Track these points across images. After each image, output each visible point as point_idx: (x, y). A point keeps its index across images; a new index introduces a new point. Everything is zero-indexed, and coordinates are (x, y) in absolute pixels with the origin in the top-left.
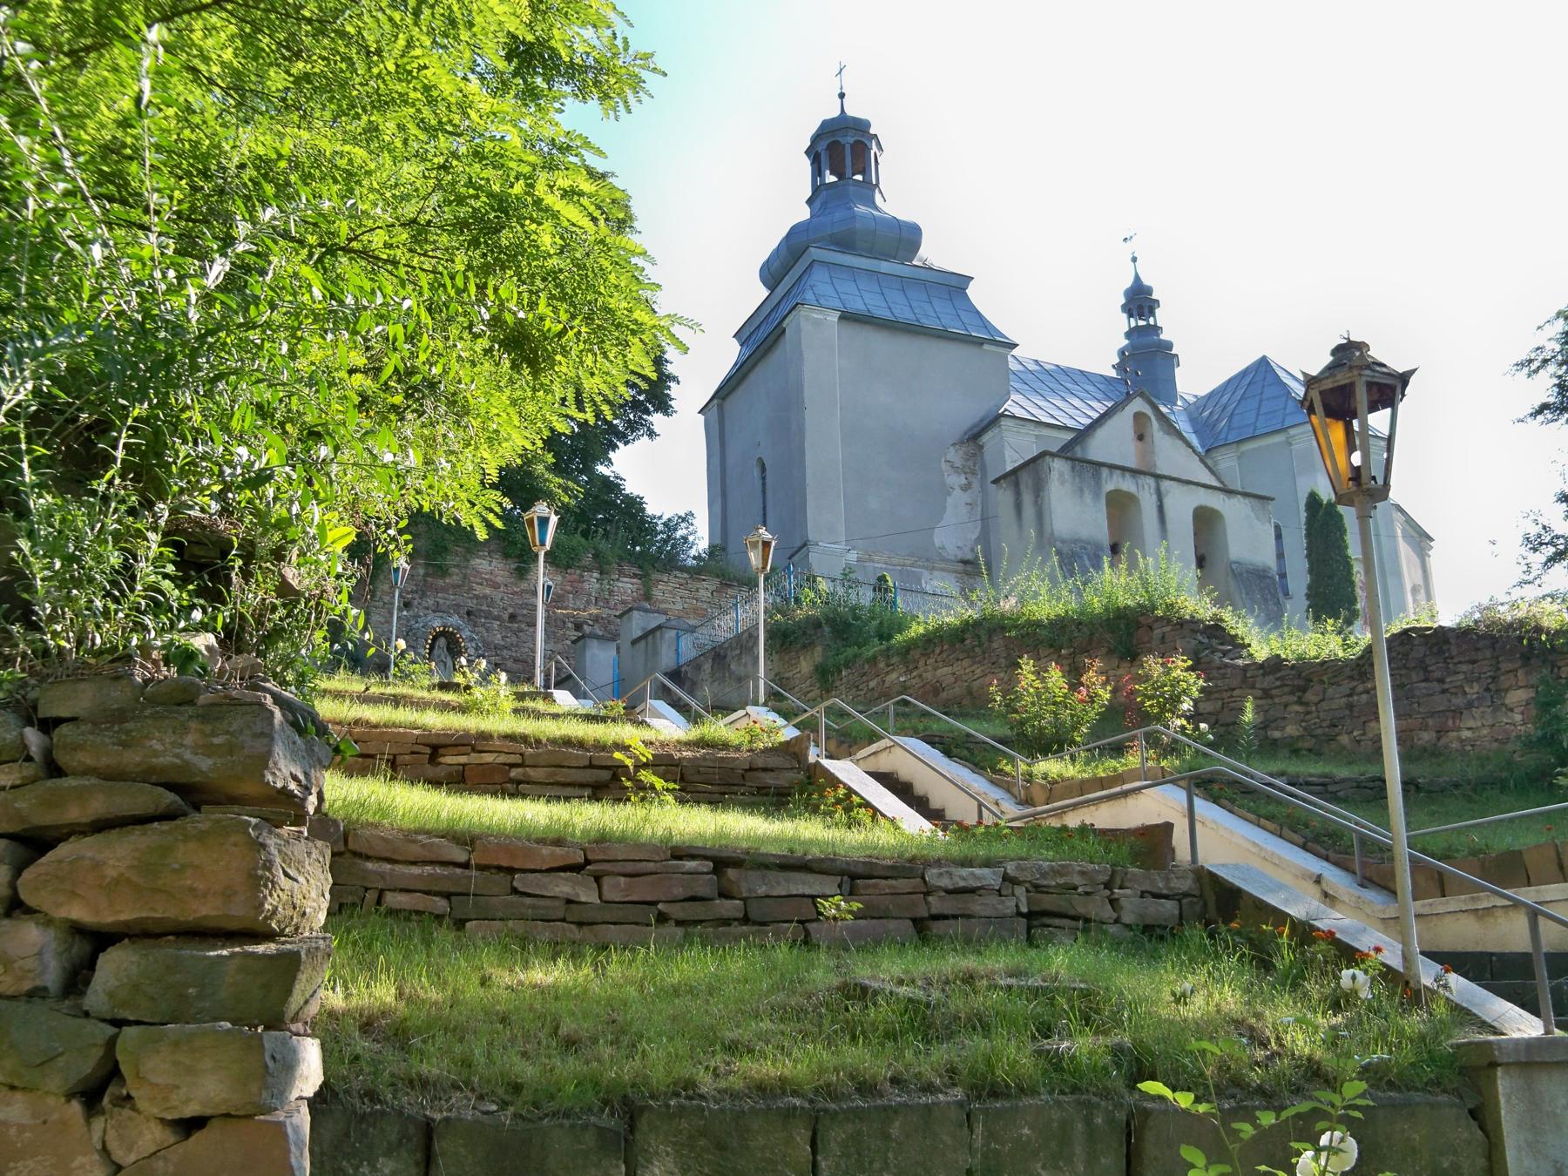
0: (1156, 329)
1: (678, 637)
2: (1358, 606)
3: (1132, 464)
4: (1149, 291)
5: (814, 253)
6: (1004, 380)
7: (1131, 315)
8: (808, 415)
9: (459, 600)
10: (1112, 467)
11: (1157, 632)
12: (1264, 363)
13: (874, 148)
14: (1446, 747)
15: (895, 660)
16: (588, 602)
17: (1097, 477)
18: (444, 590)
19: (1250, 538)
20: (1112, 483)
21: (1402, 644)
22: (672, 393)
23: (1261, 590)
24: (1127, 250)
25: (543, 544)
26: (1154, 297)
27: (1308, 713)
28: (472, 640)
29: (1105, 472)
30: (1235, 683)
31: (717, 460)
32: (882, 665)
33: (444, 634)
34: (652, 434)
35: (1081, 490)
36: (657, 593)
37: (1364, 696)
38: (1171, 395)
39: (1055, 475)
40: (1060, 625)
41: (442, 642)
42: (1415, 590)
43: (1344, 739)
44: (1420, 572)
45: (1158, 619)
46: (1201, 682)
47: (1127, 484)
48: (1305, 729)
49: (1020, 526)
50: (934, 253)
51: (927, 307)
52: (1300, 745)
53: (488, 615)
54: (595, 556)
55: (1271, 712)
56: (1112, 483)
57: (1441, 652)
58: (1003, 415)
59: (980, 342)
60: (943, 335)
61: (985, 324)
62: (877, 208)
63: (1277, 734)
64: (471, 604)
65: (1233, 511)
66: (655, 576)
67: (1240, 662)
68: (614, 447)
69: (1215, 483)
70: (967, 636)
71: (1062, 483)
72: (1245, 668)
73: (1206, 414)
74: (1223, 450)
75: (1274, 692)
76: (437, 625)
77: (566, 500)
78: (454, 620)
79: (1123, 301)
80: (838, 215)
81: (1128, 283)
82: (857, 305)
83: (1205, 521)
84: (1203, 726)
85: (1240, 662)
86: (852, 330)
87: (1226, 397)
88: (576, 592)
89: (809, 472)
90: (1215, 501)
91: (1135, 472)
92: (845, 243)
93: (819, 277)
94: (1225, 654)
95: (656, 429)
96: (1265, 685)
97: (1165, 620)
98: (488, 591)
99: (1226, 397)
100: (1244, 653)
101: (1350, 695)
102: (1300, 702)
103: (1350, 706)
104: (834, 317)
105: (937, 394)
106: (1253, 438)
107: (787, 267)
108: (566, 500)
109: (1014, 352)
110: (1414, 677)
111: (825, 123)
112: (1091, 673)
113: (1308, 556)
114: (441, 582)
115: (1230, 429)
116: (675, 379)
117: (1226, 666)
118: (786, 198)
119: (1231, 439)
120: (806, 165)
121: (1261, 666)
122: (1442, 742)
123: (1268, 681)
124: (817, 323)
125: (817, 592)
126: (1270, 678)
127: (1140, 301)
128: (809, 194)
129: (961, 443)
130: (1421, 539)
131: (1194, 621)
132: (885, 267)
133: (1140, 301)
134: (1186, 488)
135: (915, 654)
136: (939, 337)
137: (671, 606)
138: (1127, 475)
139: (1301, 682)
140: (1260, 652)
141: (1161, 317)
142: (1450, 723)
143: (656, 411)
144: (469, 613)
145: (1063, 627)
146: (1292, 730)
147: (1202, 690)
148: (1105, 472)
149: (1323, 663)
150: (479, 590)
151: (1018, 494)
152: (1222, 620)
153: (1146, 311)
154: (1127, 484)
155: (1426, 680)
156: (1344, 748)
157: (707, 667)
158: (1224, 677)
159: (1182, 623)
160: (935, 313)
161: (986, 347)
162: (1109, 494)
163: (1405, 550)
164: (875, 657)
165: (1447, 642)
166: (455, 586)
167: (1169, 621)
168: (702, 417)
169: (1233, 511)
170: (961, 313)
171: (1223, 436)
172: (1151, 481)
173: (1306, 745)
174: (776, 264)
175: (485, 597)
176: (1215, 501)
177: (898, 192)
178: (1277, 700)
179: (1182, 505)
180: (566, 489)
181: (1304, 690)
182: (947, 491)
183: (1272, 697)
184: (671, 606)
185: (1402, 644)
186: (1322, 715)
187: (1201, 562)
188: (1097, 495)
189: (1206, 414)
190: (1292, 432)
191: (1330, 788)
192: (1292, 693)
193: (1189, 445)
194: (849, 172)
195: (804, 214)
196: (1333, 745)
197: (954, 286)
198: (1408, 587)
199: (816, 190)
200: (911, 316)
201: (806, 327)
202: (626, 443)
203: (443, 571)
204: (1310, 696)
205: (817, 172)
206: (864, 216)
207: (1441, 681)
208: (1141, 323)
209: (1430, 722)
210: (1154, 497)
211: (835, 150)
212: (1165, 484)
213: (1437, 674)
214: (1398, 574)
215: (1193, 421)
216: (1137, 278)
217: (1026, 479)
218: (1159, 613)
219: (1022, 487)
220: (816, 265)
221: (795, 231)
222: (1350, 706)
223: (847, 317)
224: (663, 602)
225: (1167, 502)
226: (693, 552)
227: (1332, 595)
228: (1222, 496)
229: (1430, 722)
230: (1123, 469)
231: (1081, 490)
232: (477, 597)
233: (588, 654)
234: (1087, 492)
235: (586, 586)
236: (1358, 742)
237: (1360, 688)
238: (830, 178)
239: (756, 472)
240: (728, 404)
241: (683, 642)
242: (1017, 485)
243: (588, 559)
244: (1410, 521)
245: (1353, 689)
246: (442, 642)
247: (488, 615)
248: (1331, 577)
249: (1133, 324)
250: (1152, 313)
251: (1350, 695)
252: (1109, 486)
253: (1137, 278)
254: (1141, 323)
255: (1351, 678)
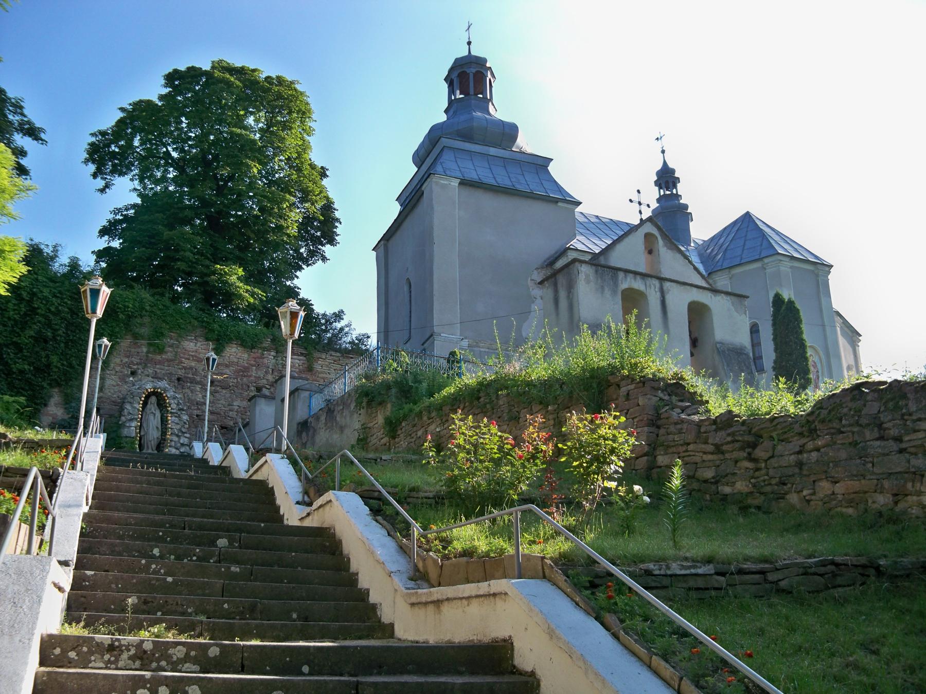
0: (678, 196)
1: (311, 397)
2: (811, 376)
3: (642, 269)
4: (673, 171)
5: (445, 141)
6: (572, 226)
7: (660, 188)
8: (435, 247)
9: (172, 370)
10: (627, 271)
11: (624, 390)
12: (747, 215)
13: (489, 76)
14: (904, 512)
15: (434, 414)
16: (266, 372)
17: (615, 279)
18: (160, 363)
19: (731, 325)
20: (628, 282)
21: (853, 399)
22: (338, 231)
23: (736, 364)
24: (658, 146)
25: (94, 311)
26: (676, 175)
27: (757, 469)
28: (175, 398)
29: (621, 275)
30: (690, 437)
31: (383, 280)
32: (425, 418)
33: (154, 393)
34: (324, 259)
35: (602, 287)
36: (317, 367)
37: (814, 455)
38: (685, 236)
39: (582, 276)
40: (547, 385)
41: (153, 399)
42: (849, 368)
43: (793, 498)
44: (852, 356)
45: (624, 378)
46: (632, 440)
47: (638, 284)
48: (754, 486)
49: (557, 314)
50: (526, 143)
51: (521, 177)
52: (750, 501)
53: (193, 381)
54: (273, 340)
55: (722, 467)
56: (628, 282)
57: (897, 407)
58: (569, 248)
59: (556, 201)
60: (531, 196)
61: (560, 189)
62: (489, 114)
63: (727, 490)
64: (181, 373)
65: (718, 305)
66: (316, 355)
67: (696, 418)
68: (300, 268)
69: (704, 284)
70: (482, 394)
71: (588, 281)
72: (699, 424)
73: (709, 251)
74: (719, 273)
75: (725, 448)
76: (149, 387)
77: (252, 300)
78: (163, 384)
79: (656, 178)
80: (463, 118)
81: (659, 166)
82: (472, 175)
83: (697, 312)
84: (636, 488)
85: (696, 418)
86: (467, 191)
87: (723, 239)
88: (258, 366)
89: (436, 286)
90: (705, 298)
91: (644, 276)
92: (467, 135)
93: (447, 157)
94: (683, 410)
95: (327, 255)
96: (717, 441)
97: (630, 378)
98: (193, 364)
99: (723, 239)
100: (702, 409)
101: (800, 452)
102: (750, 458)
103: (800, 465)
104: (455, 183)
105: (526, 237)
106: (737, 266)
107: (429, 154)
108: (252, 300)
109: (579, 209)
110: (868, 434)
111: (457, 60)
112: (531, 429)
113: (774, 340)
114: (158, 357)
115: (724, 259)
116: (338, 220)
117: (682, 421)
118: (433, 106)
119: (726, 265)
120: (445, 87)
121: (715, 422)
122: (901, 506)
123: (720, 437)
124: (444, 187)
125: (400, 363)
126: (722, 434)
127: (666, 178)
128: (446, 105)
129: (542, 268)
130: (853, 335)
131: (655, 379)
132: (493, 151)
133: (666, 178)
134: (683, 287)
135: (446, 409)
136: (527, 197)
137: (328, 376)
138: (638, 277)
139: (750, 439)
140: (716, 408)
141: (681, 189)
142: (909, 485)
143: (327, 243)
144: (179, 379)
145: (551, 386)
146: (741, 486)
147: (634, 449)
148: (621, 275)
149: (773, 419)
150: (187, 363)
151: (556, 291)
152: (682, 379)
153: (671, 185)
154: (638, 284)
155: (881, 438)
156: (793, 507)
157: (323, 418)
158: (680, 432)
159: (644, 381)
160: (529, 182)
161: (560, 204)
162: (624, 292)
163: (842, 341)
164: (421, 412)
165: (904, 396)
166: (169, 360)
167: (633, 380)
168: (374, 253)
169: (718, 305)
170: (544, 182)
171: (720, 264)
172: (656, 283)
173: (756, 502)
174: (423, 151)
175: (191, 368)
176: (705, 298)
177: (503, 106)
178: (727, 456)
179: (679, 300)
180: (253, 294)
181: (754, 446)
182: (532, 300)
183: (723, 453)
184: (328, 376)
185: (853, 399)
186: (771, 472)
187: (694, 342)
188: (614, 292)
189: (709, 251)
190: (766, 261)
191: (772, 577)
192: (742, 449)
193: (696, 269)
194: (472, 91)
195: (443, 118)
196: (782, 504)
197: (541, 164)
198: (845, 366)
199: (450, 102)
200: (510, 183)
201: (436, 189)
202: (308, 266)
203: (160, 350)
204: (759, 453)
205: (451, 91)
206: (479, 118)
207: (898, 439)
208: (668, 192)
209: (886, 484)
210: (658, 294)
211: (463, 76)
212: (667, 285)
213: (894, 432)
214: (839, 357)
215: (701, 256)
216: (665, 162)
217: (561, 279)
218: (626, 372)
219: (559, 286)
220: (445, 150)
221: (434, 129)
222: (800, 465)
223: (464, 183)
224: (322, 373)
225: (669, 298)
226: (348, 339)
227: (793, 366)
228: (709, 294)
229: (886, 484)
230: (636, 273)
231: (602, 287)
232: (185, 368)
233: (258, 409)
234: (606, 289)
235: (266, 361)
236: (808, 501)
237: (810, 446)
238: (459, 96)
239: (406, 288)
240: (391, 242)
241: (314, 400)
242: (555, 285)
243: (267, 343)
244: (845, 323)
245: (803, 446)
246: (153, 399)
247: (193, 381)
248: (790, 354)
249: (662, 193)
250: (675, 186)
251: (800, 452)
252: (624, 286)
253: (665, 162)
254: (668, 192)
255: (801, 434)
